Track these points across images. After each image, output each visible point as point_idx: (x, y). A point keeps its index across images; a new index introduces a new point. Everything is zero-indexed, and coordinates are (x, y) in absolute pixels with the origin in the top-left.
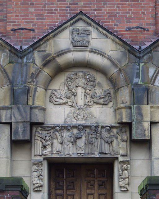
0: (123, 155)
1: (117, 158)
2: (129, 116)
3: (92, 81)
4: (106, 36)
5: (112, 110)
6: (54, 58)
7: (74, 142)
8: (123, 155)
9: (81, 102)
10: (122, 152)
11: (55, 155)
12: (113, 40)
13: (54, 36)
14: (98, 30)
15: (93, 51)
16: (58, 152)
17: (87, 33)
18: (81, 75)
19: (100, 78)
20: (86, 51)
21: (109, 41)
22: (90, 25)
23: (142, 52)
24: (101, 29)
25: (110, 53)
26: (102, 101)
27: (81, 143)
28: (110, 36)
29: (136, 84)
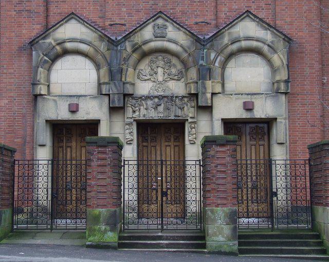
3: (169, 64)
4: (180, 30)
9: (160, 78)
11: (142, 118)
15: (170, 41)
17: (165, 27)
20: (164, 41)
21: (181, 33)
22: (167, 21)
26: (176, 77)
27: (161, 108)
28: (182, 29)
29: (201, 65)
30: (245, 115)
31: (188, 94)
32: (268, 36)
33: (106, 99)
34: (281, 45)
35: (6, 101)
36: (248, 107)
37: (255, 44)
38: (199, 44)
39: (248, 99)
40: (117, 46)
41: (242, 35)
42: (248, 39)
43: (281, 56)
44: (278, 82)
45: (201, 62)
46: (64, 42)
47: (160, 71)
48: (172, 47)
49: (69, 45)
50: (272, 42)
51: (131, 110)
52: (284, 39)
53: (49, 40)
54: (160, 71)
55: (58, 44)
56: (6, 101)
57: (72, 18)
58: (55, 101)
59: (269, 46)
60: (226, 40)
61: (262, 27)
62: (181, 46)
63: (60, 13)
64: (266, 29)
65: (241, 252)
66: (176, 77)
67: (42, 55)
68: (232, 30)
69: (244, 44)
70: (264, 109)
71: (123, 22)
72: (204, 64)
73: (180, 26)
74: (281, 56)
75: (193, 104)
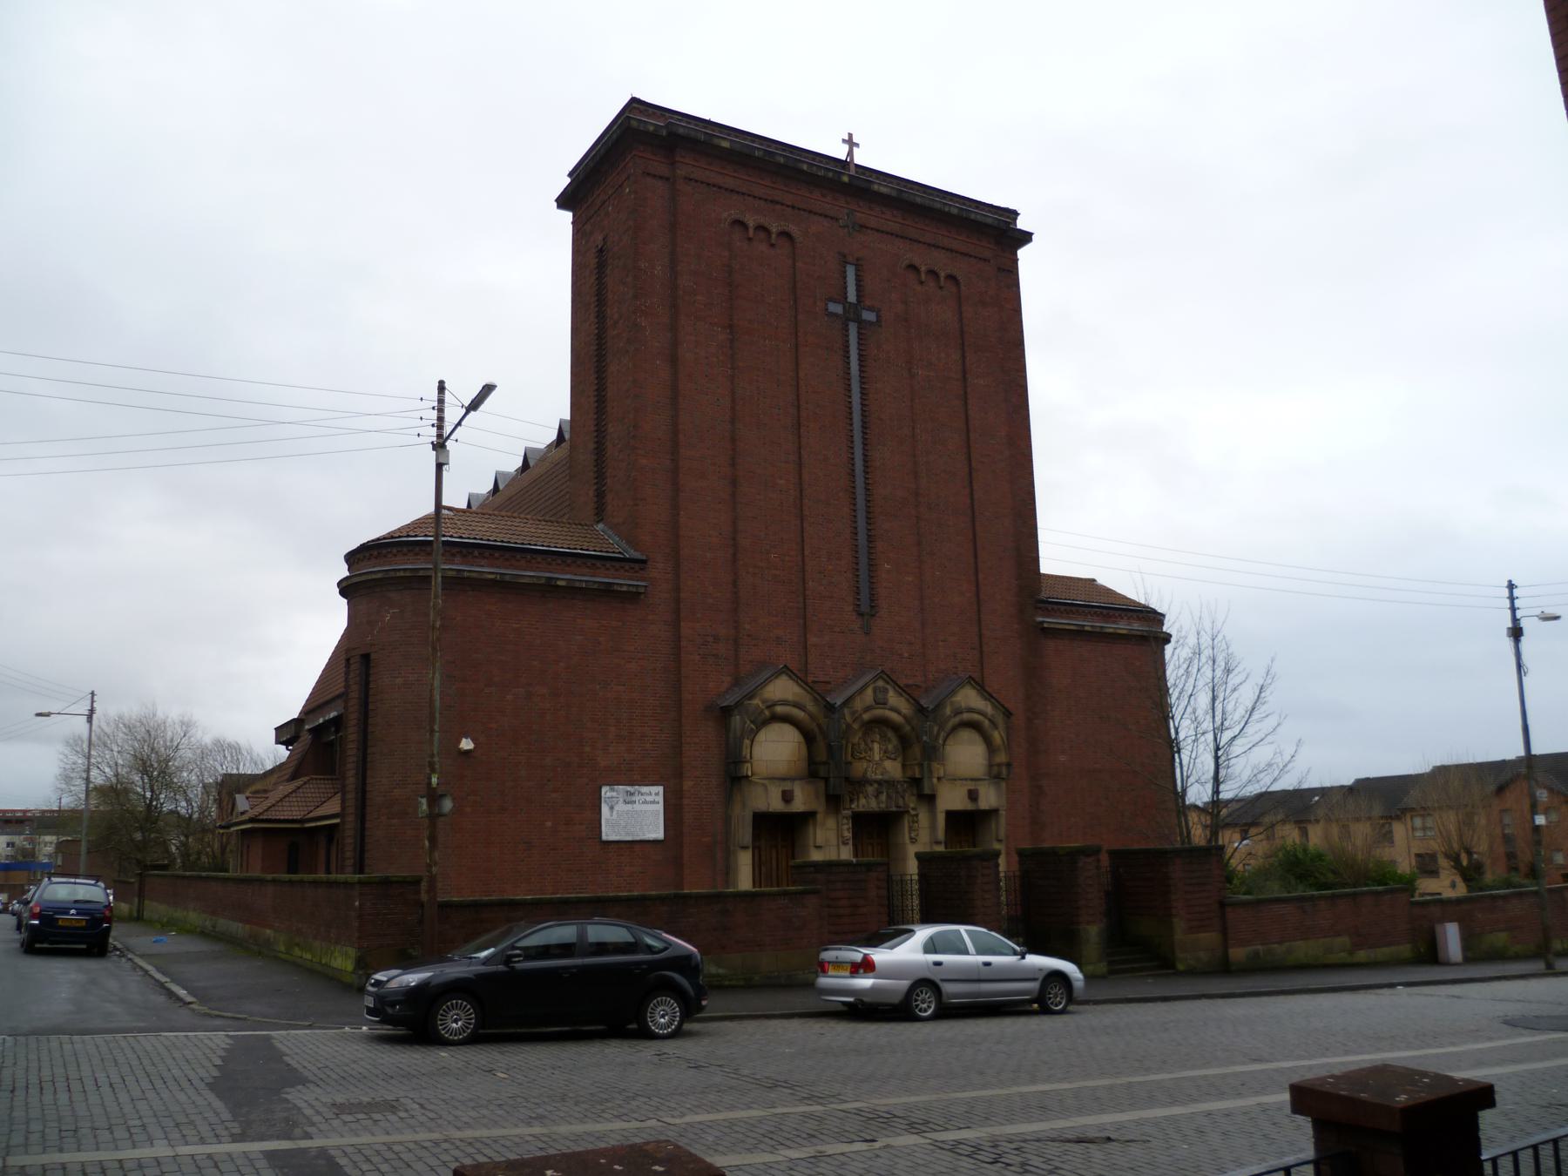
0: (913, 809)
1: (908, 812)
2: (372, 665)
3: (884, 738)
4: (901, 695)
5: (900, 765)
6: (861, 715)
7: (877, 797)
8: (913, 809)
9: (877, 757)
10: (912, 805)
11: (861, 809)
12: (908, 700)
13: (761, 689)
14: (797, 682)
15: (893, 709)
16: (863, 806)
17: (886, 691)
18: (1457, 815)
19: (890, 734)
20: (885, 709)
21: (903, 699)
22: (888, 683)
23: (815, 697)
24: (897, 688)
25: (904, 711)
26: (893, 756)
27: (883, 797)
28: (904, 694)
29: (925, 742)
30: (969, 806)
31: (909, 778)
32: (988, 708)
33: (822, 784)
34: (1000, 720)
35: (692, 783)
36: (973, 796)
37: (976, 717)
38: (1220, 775)
39: (971, 786)
40: (833, 713)
41: (963, 705)
42: (970, 710)
43: (1002, 733)
44: (999, 765)
45: (925, 738)
46: (775, 704)
47: (876, 746)
48: (894, 716)
49: (779, 709)
50: (992, 716)
51: (848, 799)
52: (1004, 713)
53: (756, 701)
54: (876, 746)
55: (768, 707)
56: (692, 783)
57: (784, 672)
58: (763, 785)
59: (990, 720)
60: (948, 711)
61: (982, 696)
62: (905, 717)
63: (750, 661)
64: (986, 699)
65: (1112, 972)
66: (893, 756)
67: (748, 722)
68: (954, 699)
69: (966, 716)
70: (989, 798)
71: (827, 679)
72: (928, 741)
73: (903, 690)
74: (1002, 733)
75: (1475, 856)
